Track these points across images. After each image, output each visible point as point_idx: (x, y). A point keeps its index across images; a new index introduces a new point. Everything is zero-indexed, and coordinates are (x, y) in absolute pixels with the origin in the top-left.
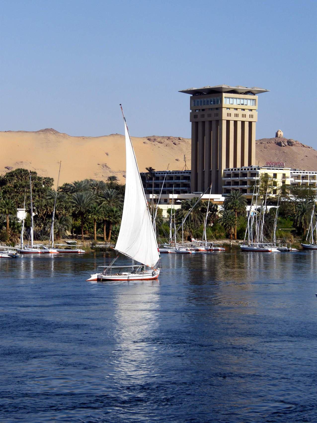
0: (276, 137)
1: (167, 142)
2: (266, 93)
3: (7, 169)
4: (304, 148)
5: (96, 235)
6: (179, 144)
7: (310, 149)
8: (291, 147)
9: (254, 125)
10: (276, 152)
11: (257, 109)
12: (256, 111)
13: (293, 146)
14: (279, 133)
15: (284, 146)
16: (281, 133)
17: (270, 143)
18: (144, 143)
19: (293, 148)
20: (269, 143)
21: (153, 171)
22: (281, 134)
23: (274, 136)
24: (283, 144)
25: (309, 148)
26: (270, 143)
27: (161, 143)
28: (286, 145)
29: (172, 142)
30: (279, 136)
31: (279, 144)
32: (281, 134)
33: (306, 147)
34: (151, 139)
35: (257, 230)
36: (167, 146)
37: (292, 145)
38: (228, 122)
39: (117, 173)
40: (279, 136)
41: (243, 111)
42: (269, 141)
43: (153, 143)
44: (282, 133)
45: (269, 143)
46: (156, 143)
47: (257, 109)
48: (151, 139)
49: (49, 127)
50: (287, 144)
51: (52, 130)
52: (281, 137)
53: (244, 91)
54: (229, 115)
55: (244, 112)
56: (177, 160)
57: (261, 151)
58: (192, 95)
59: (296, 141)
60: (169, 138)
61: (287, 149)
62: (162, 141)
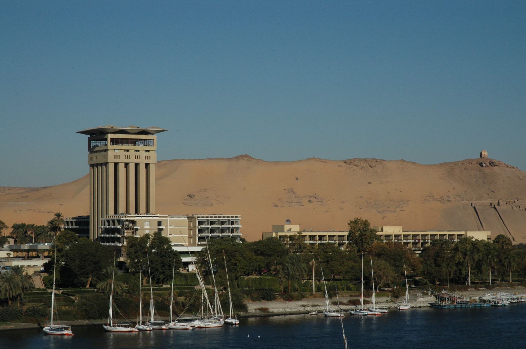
0: (480, 157)
1: (363, 164)
2: (162, 133)
3: (190, 197)
4: (507, 169)
5: (151, 288)
6: (375, 166)
7: (514, 169)
8: (493, 168)
9: (152, 168)
10: (476, 173)
11: (156, 150)
12: (155, 152)
13: (496, 166)
14: (483, 153)
15: (486, 167)
16: (485, 153)
17: (471, 163)
18: (339, 166)
19: (495, 168)
20: (470, 163)
21: (35, 226)
22: (485, 154)
23: (479, 157)
24: (484, 165)
25: (514, 168)
26: (471, 163)
27: (357, 166)
28: (487, 166)
29: (369, 164)
30: (483, 156)
31: (481, 164)
32: (485, 154)
33: (510, 168)
34: (347, 162)
35: (193, 299)
36: (362, 168)
37: (494, 166)
38: (116, 164)
39: (303, 198)
40: (483, 157)
41: (147, 153)
42: (470, 162)
43: (349, 166)
44: (486, 153)
45: (470, 163)
46: (352, 166)
47: (156, 150)
48: (347, 162)
49: (244, 154)
50: (488, 164)
51: (246, 156)
52: (485, 157)
53: (136, 132)
54: (116, 157)
55: (137, 154)
56: (369, 183)
57: (461, 172)
58: (89, 136)
59: (499, 162)
60: (366, 161)
61: (487, 170)
62: (358, 164)
